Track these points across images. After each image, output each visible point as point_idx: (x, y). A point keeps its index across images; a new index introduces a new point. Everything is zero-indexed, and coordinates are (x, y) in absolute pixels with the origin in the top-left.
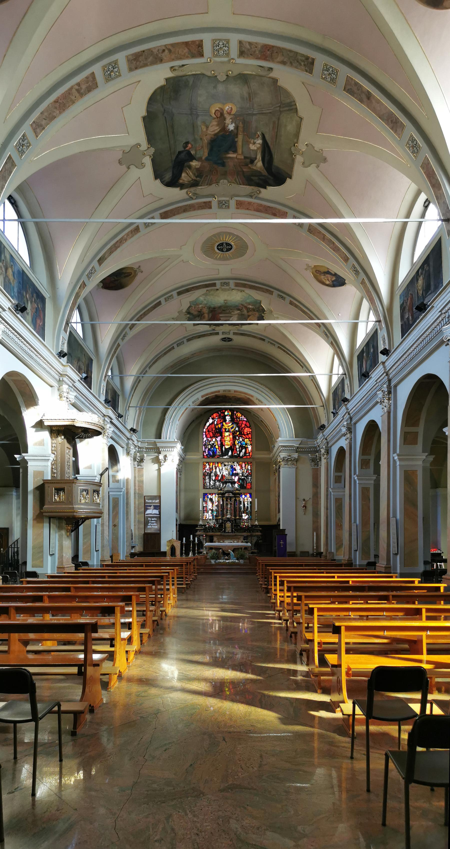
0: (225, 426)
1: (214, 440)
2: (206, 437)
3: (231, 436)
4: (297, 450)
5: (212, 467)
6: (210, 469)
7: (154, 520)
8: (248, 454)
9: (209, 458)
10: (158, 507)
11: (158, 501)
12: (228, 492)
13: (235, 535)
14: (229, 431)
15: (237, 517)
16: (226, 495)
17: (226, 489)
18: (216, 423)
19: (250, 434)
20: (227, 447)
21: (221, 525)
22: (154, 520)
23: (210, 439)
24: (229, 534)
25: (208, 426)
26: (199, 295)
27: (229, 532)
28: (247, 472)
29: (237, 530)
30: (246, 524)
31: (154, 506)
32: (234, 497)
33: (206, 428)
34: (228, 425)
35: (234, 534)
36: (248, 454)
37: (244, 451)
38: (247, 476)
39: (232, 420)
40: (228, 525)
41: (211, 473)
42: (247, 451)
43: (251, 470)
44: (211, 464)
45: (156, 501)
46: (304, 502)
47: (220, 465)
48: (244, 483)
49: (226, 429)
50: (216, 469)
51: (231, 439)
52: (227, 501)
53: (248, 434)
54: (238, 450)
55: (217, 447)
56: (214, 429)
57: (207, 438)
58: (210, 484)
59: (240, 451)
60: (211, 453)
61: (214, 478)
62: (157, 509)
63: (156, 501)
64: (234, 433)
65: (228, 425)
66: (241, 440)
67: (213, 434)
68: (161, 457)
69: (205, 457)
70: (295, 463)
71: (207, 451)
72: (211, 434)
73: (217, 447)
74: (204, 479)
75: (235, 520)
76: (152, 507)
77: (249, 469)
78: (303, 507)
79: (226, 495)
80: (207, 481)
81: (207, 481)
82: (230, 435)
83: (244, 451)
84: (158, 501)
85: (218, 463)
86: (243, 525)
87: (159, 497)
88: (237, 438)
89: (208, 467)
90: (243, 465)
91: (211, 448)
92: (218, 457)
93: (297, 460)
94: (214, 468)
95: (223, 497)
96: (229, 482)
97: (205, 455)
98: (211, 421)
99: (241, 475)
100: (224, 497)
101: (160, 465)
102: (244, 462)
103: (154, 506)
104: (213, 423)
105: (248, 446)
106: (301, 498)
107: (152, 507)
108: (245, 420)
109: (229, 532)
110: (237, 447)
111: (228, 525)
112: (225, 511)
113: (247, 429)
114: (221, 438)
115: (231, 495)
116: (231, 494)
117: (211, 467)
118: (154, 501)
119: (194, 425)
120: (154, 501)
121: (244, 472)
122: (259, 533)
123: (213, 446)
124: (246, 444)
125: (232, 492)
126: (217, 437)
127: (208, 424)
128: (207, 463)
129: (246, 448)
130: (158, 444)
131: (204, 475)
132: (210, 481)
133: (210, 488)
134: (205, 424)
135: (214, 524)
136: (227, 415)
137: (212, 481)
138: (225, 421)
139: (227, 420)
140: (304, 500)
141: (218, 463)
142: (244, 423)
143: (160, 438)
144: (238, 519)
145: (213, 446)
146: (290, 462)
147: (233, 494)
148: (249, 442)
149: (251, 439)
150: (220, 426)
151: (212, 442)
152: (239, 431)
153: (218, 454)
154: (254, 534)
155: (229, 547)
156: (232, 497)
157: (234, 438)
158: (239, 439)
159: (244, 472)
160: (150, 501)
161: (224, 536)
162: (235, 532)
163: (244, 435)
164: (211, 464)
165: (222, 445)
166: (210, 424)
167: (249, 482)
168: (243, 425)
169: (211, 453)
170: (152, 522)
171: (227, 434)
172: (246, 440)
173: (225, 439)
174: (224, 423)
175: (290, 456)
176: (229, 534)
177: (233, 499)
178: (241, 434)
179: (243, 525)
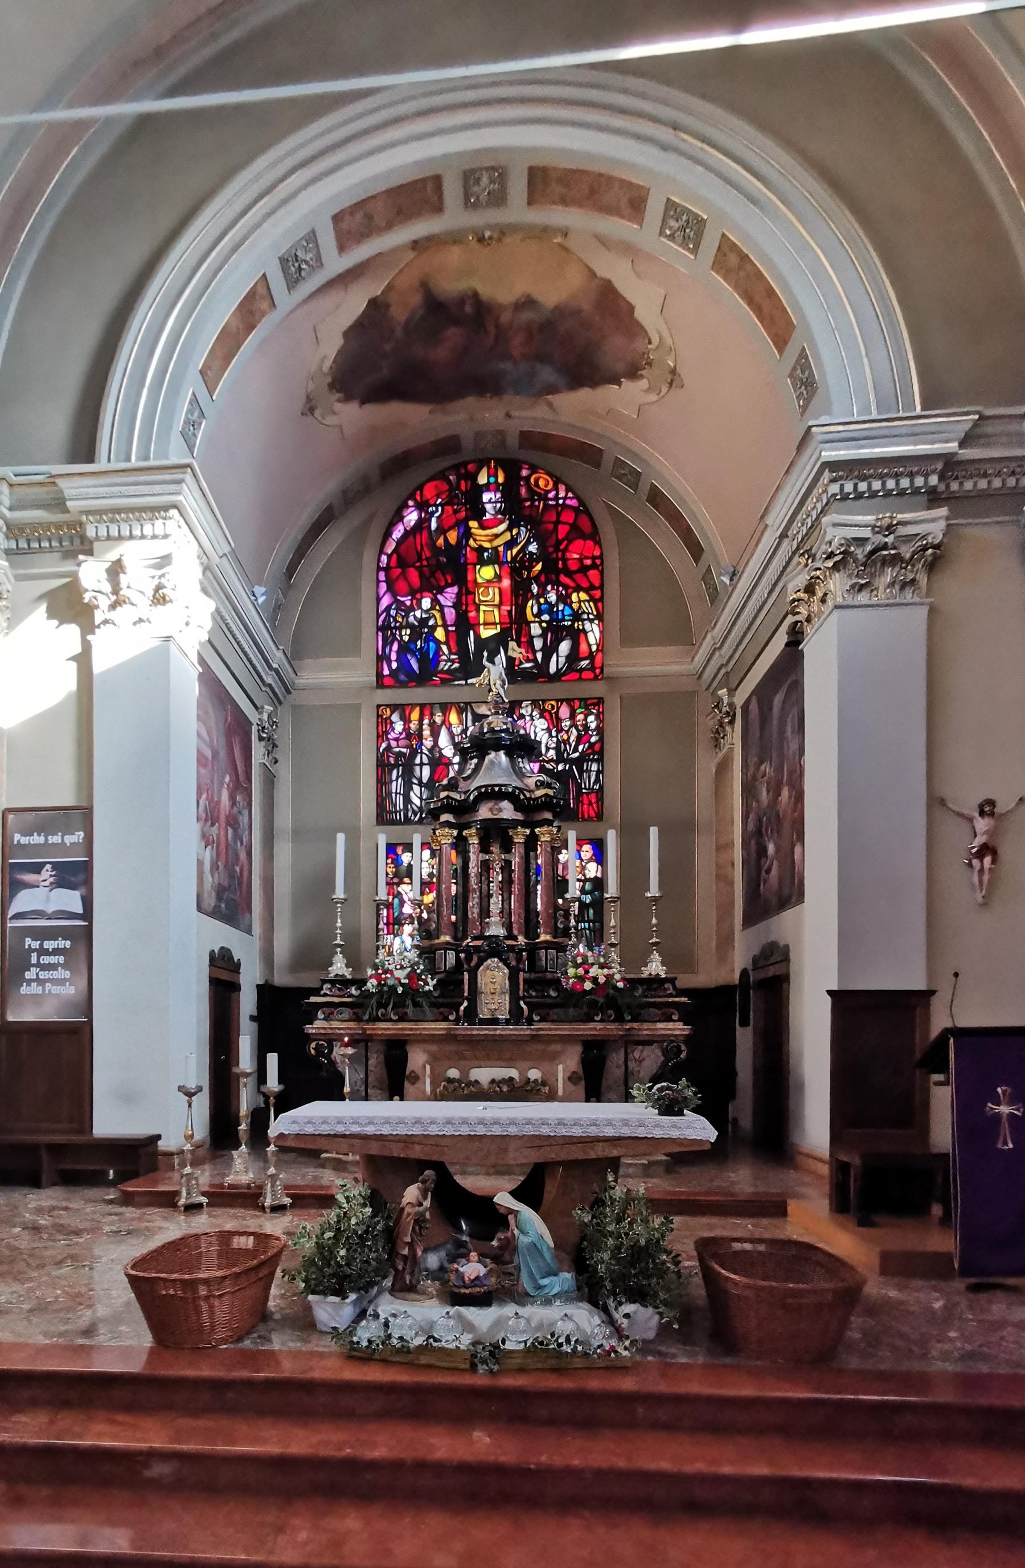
0: (481, 536)
1: (426, 603)
2: (390, 589)
3: (506, 583)
4: (946, 481)
5: (420, 729)
6: (409, 736)
7: (56, 952)
8: (584, 663)
9: (403, 685)
10: (76, 874)
11: (79, 836)
12: (492, 794)
13: (535, 1038)
14: (495, 559)
15: (543, 938)
16: (484, 812)
17: (482, 780)
18: (434, 525)
19: (594, 566)
20: (486, 633)
21: (450, 983)
22: (56, 952)
23: (407, 600)
24: (500, 1030)
25: (400, 542)
26: (424, 479)
27: (494, 1021)
28: (579, 740)
29: (543, 1010)
30: (594, 971)
31: (55, 866)
32: (524, 824)
33: (390, 548)
34: (491, 534)
35: (524, 1030)
36: (584, 663)
37: (565, 647)
38: (579, 762)
39: (514, 510)
40: (493, 978)
41: (414, 753)
42: (583, 647)
43: (600, 730)
44: (415, 715)
45: (69, 839)
46: (982, 824)
47: (453, 718)
48: (567, 791)
49: (481, 549)
50: (435, 734)
51: (507, 596)
52: (484, 848)
53: (584, 569)
54: (538, 644)
55: (440, 634)
56: (427, 553)
57: (394, 595)
58: (407, 800)
59: (550, 650)
60: (415, 665)
61: (426, 772)
62: (73, 887)
63: (69, 839)
64: (518, 570)
65: (491, 534)
66: (552, 597)
67: (422, 576)
68: (91, 573)
69: (387, 681)
70: (923, 579)
71: (394, 656)
72: (414, 576)
73: (440, 634)
74: (382, 782)
75: (532, 949)
76: (47, 873)
77: (593, 726)
78: (980, 854)
79: (484, 812)
80: (396, 786)
81: (396, 786)
82: (498, 578)
83: (565, 647)
84: (79, 836)
85: (445, 708)
86: (581, 979)
87: (81, 815)
88: (535, 589)
89: (399, 727)
90: (564, 712)
91: (413, 639)
92: (444, 682)
93: (935, 558)
94: (426, 732)
95: (461, 827)
96: (497, 746)
97: (386, 672)
98: (412, 517)
99: (552, 753)
100: (468, 826)
101: (88, 627)
102: (569, 701)
103: (55, 866)
104: (422, 524)
105: (587, 626)
106: (966, 797)
107: (47, 873)
108: (574, 503)
109: (494, 1021)
110: (535, 629)
111: (493, 978)
112: (473, 903)
113: (579, 543)
114: (459, 595)
115: (507, 811)
116: (506, 805)
117: (413, 726)
118: (55, 839)
119: (333, 540)
120: (55, 839)
121: (567, 742)
122: (677, 1028)
123: (422, 629)
124: (577, 616)
125: (512, 797)
126: (441, 591)
127: (397, 533)
128: (394, 708)
129: (577, 636)
130: (62, 483)
131: (383, 767)
132: (408, 787)
133: (407, 821)
134: (388, 534)
135: (412, 976)
136: (487, 487)
137: (416, 788)
138: (478, 512)
139: (489, 507)
140: (987, 808)
141: (445, 708)
142: (568, 517)
143: (90, 458)
144: (547, 945)
145: (422, 629)
146: (889, 574)
147: (518, 806)
148: (589, 607)
149: (597, 594)
150: (453, 536)
151: (418, 613)
152: (542, 556)
153: (444, 666)
154: (645, 1029)
155: (490, 1149)
156: (514, 824)
157: (519, 593)
158: (543, 593)
159: (567, 742)
160: (37, 839)
161: (472, 1042)
162: (530, 1021)
163: (569, 574)
164: (415, 715)
165: (465, 623)
166: (407, 533)
167: (591, 790)
168: (563, 531)
169: (415, 665)
170: (46, 960)
171: (487, 572)
172: (574, 597)
173: (481, 596)
174: (473, 524)
175: (890, 529)
176: (500, 1030)
177: (520, 835)
178: (552, 574)
179: (581, 979)
